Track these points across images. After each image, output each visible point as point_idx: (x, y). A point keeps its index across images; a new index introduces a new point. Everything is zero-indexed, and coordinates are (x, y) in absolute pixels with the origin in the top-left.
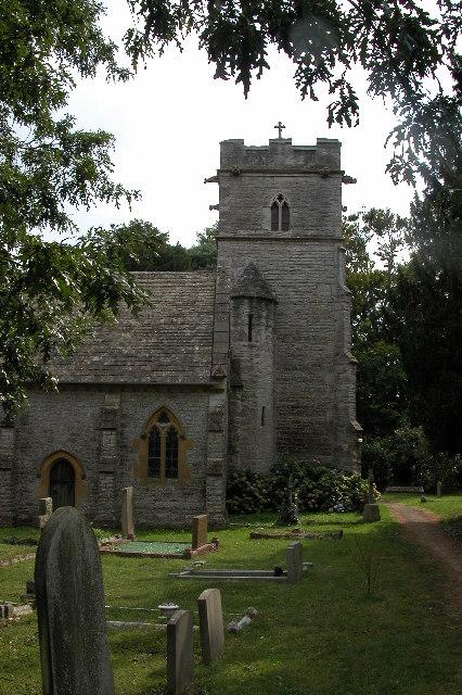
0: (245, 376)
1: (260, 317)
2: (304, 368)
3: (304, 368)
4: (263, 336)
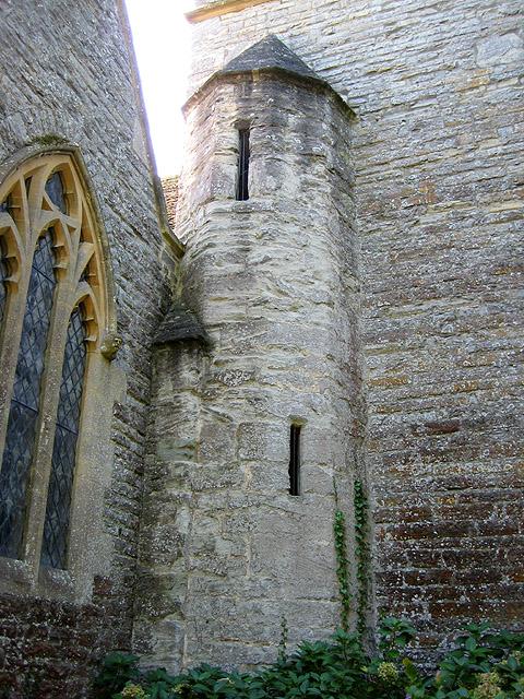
0: (216, 310)
1: (275, 124)
2: (465, 286)
3: (465, 286)
4: (284, 179)
